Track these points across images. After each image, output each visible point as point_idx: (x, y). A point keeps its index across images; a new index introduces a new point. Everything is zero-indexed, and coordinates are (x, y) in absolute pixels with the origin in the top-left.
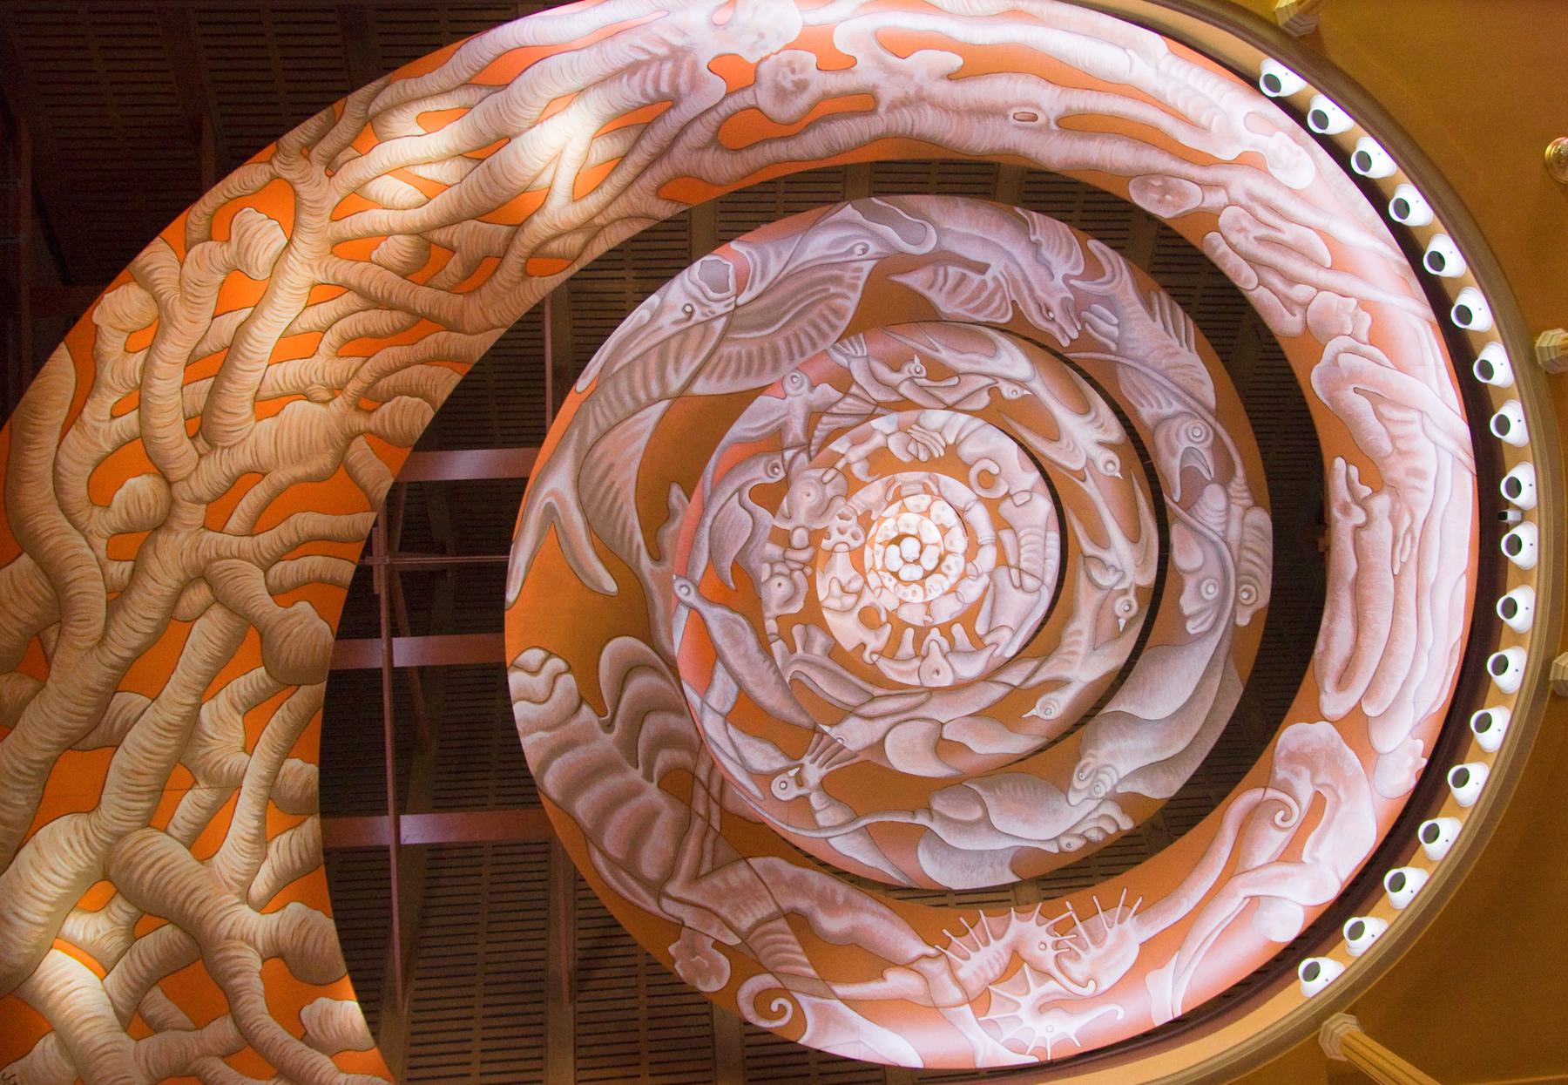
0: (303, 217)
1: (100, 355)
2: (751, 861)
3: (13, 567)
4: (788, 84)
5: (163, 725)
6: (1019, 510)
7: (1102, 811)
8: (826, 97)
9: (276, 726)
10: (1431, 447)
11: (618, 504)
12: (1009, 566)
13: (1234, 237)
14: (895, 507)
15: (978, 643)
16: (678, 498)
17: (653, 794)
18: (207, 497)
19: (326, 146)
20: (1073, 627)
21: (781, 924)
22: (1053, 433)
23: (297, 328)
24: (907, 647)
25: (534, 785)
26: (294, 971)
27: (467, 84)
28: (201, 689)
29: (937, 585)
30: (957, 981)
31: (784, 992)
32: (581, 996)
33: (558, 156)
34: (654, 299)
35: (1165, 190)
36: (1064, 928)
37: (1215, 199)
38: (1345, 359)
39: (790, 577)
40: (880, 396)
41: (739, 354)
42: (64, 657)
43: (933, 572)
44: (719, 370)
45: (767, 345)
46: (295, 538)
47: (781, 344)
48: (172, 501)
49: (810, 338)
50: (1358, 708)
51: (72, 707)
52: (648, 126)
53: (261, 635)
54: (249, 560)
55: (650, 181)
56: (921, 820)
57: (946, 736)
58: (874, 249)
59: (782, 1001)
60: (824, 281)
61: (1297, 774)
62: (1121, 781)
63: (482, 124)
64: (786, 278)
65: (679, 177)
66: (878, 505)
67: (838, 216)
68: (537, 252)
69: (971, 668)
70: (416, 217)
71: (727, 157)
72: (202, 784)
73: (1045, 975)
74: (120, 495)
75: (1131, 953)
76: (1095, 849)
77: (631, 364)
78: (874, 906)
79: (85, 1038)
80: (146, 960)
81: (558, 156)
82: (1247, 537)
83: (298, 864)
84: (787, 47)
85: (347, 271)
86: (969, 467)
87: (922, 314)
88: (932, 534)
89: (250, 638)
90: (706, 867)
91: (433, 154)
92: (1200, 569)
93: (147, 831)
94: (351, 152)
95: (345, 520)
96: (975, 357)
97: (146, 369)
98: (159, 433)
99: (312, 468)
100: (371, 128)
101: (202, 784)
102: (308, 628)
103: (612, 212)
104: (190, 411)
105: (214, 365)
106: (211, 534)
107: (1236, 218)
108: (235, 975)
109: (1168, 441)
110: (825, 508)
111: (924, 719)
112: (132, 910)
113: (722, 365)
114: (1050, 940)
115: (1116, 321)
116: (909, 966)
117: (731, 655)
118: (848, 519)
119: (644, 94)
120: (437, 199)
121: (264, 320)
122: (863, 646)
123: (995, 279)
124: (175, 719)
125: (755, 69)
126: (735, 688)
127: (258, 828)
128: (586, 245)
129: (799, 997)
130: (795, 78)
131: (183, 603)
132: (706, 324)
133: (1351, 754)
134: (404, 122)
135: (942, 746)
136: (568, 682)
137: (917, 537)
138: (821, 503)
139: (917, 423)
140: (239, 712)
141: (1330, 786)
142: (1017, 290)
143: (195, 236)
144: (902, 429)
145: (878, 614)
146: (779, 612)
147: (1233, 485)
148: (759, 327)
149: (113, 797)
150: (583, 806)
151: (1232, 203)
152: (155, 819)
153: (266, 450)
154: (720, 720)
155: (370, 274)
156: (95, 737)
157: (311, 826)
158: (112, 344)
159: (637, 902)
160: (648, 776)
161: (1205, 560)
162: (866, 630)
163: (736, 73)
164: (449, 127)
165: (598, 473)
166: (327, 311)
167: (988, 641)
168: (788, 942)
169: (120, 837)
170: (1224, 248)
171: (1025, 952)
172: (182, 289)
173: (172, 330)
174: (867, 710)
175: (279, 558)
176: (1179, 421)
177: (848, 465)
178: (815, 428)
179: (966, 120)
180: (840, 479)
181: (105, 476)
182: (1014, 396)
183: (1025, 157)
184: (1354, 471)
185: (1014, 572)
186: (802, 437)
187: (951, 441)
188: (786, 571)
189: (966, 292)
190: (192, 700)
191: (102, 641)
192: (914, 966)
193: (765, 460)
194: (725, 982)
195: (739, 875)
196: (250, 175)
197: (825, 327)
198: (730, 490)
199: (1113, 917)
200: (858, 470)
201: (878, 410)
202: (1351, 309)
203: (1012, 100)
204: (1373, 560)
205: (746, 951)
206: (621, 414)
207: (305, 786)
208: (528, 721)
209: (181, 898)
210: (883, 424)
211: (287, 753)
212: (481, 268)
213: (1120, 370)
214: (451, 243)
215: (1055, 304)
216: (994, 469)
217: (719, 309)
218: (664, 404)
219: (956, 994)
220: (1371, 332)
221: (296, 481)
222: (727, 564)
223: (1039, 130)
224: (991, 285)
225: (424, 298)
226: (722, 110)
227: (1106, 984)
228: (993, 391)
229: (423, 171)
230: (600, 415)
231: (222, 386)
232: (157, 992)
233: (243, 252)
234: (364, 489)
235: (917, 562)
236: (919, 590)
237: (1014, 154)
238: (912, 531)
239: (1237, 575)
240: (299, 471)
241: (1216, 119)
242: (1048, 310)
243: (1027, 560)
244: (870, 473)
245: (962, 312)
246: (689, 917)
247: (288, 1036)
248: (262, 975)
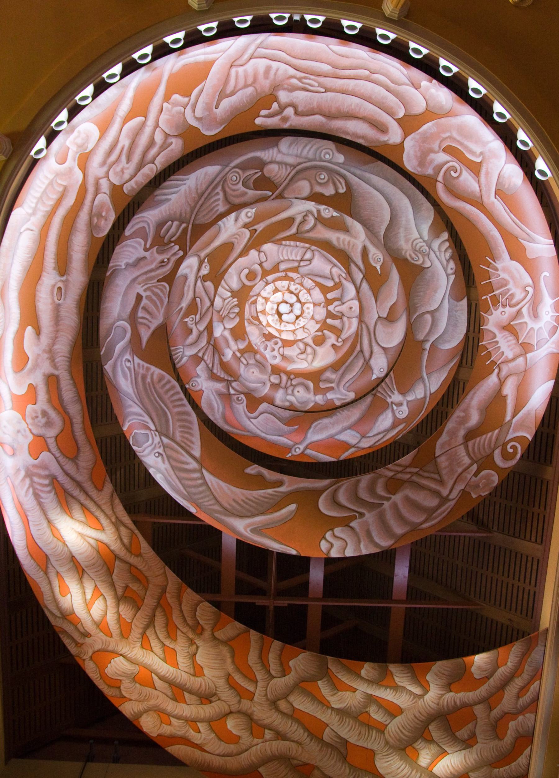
0: (110, 648)
1: (171, 735)
2: (436, 455)
3: (264, 774)
4: (44, 421)
5: (339, 723)
6: (269, 258)
7: (436, 249)
8: (50, 401)
9: (345, 678)
10: (253, 61)
11: (254, 499)
12: (299, 266)
13: (127, 176)
14: (262, 318)
15: (338, 285)
16: (252, 470)
17: (397, 498)
18: (239, 698)
19: (76, 636)
20: (335, 242)
21: (470, 444)
22: (228, 246)
23: (162, 656)
24: (336, 323)
25: (387, 551)
26: (458, 679)
27: (46, 573)
28: (325, 707)
29: (304, 296)
30: (514, 359)
31: (505, 445)
32: (490, 525)
33: (81, 535)
34: (151, 471)
35: (99, 216)
36: (496, 301)
37: (105, 185)
38: (198, 113)
39: (295, 386)
41: (181, 432)
42: (305, 758)
43: (298, 297)
45: (177, 417)
46: (260, 664)
47: (176, 410)
48: (239, 712)
49: (173, 395)
50: (399, 121)
51: (327, 757)
52: (65, 491)
53: (303, 681)
54: (269, 683)
55: (93, 493)
56: (427, 346)
57: (385, 315)
58: (128, 356)
59: (509, 447)
61: (432, 161)
63: (67, 567)
65: (91, 479)
66: (260, 330)
67: (111, 374)
68: (128, 549)
70: (111, 601)
71: (81, 454)
72: (368, 709)
73: (519, 313)
74: (234, 732)
75: (516, 266)
76: (456, 254)
77: (183, 485)
78: (468, 397)
79: (473, 762)
80: (443, 737)
81: (81, 535)
82: (295, 152)
83: (409, 675)
84: (24, 419)
85: (136, 633)
86: (244, 285)
87: (163, 334)
88: (278, 296)
89: (304, 685)
90: (436, 476)
91: (80, 591)
92: (310, 182)
93: (386, 732)
94: (79, 626)
95: (252, 642)
97: (178, 718)
98: (207, 714)
99: (228, 655)
100: (68, 616)
101: (368, 709)
102: (302, 662)
103: (109, 512)
104: (199, 702)
105: (177, 690)
106: (255, 698)
107: (116, 173)
108: (455, 703)
110: (261, 365)
112: (420, 741)
113: (186, 441)
114: (501, 309)
115: (170, 223)
116: (502, 383)
117: (332, 431)
118: (267, 346)
119: (50, 492)
120: (102, 591)
121: (156, 668)
123: (145, 290)
124: (337, 718)
125: (36, 436)
126: (349, 431)
127: (391, 689)
129: (508, 438)
130: (40, 416)
131: (285, 711)
132: (165, 446)
133: (425, 127)
134: (65, 602)
136: (338, 531)
137: (279, 304)
138: (259, 367)
140: (337, 693)
141: (441, 141)
142: (152, 278)
143: (118, 693)
144: (222, 320)
146: (312, 393)
147: (265, 158)
148: (167, 421)
149: (369, 744)
150: (399, 530)
151: (107, 176)
152: (381, 729)
153: (217, 673)
154: (364, 440)
155: (137, 623)
156: (342, 749)
157: (393, 668)
158: (166, 730)
159: (449, 509)
160: (388, 499)
161: (305, 179)
162: (326, 343)
163: (38, 445)
164: (67, 582)
165: (239, 508)
166: (154, 643)
167: (337, 280)
168: (480, 441)
169: (387, 743)
170: (132, 183)
171: (505, 323)
172: (143, 701)
173: (161, 706)
174: (367, 354)
175: (268, 672)
176: (227, 189)
177: (239, 351)
178: (219, 377)
179: (61, 327)
180: (246, 355)
181: (225, 737)
182: (208, 267)
183: (81, 296)
184: (264, 112)
186: (224, 384)
187: (229, 294)
188: (292, 388)
189: (152, 308)
190: (330, 711)
191: (298, 743)
192: (502, 380)
193: (234, 404)
194: (496, 474)
195: (443, 462)
196: (90, 669)
197: (168, 387)
199: (494, 274)
200: (242, 346)
201: (212, 343)
202: (170, 106)
203: (50, 301)
204: (315, 104)
205: (480, 461)
206: (208, 493)
207: (373, 668)
208: (355, 551)
209: (418, 722)
211: (358, 676)
212: (135, 574)
213: (197, 222)
214: (123, 587)
215: (159, 258)
216: (246, 271)
217: (157, 439)
219: (520, 360)
220: (183, 95)
221: (233, 662)
222: (286, 428)
223: (66, 286)
224: (148, 293)
225: (149, 601)
226: (58, 455)
227: (529, 280)
228: (205, 279)
229: (89, 596)
230: (208, 502)
231: (188, 689)
232: (457, 734)
233: (127, 676)
234: (238, 635)
235: (292, 305)
237: (79, 302)
238: (275, 306)
239: (315, 160)
240: (229, 661)
241: (59, 182)
242: (163, 262)
243: (296, 257)
244: (244, 340)
245: (162, 311)
246: (460, 487)
247: (487, 684)
248: (457, 693)
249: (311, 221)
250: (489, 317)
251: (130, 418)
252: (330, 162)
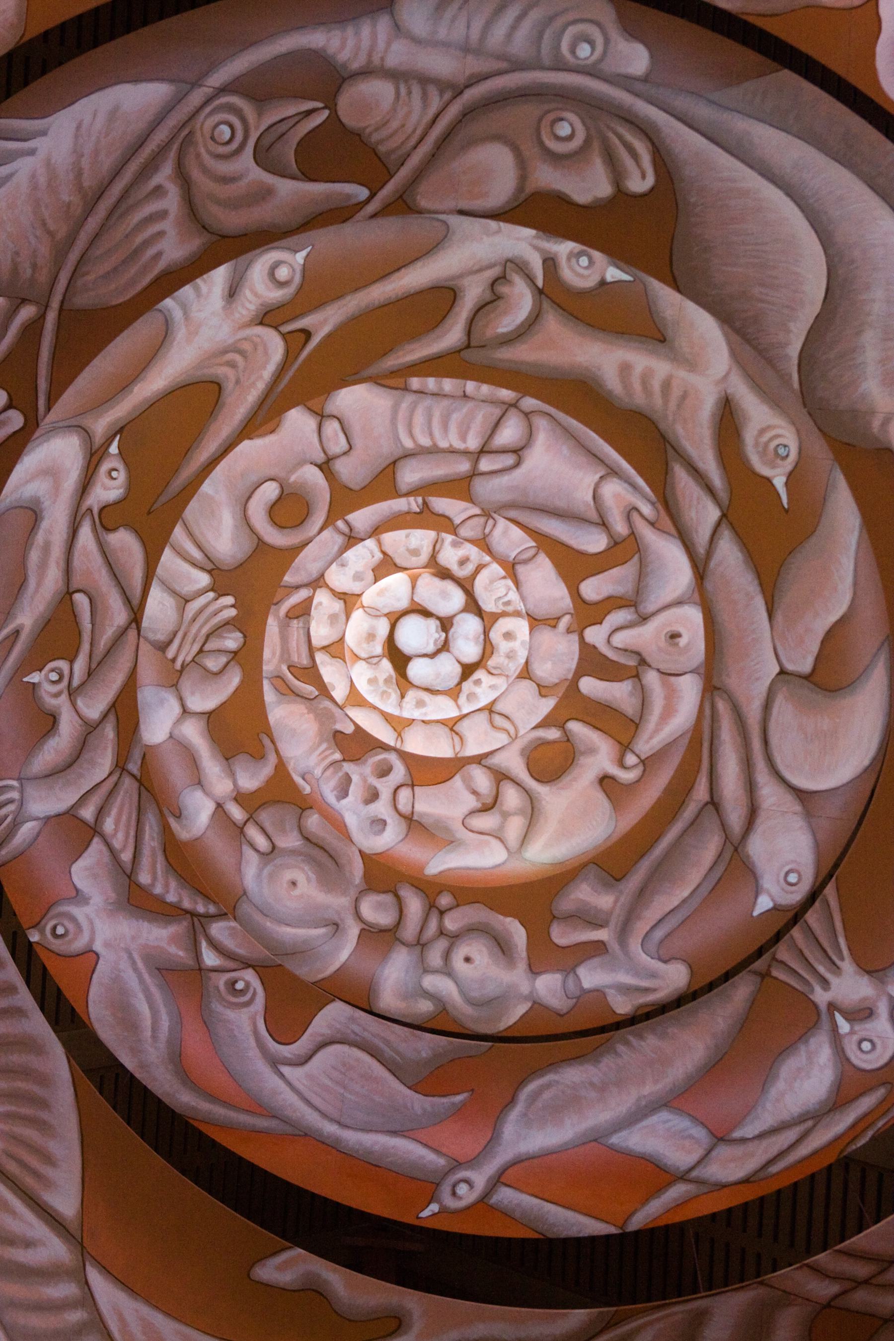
6: (358, 442)
12: (474, 473)
15: (625, 549)
16: (280, 1268)
20: (612, 382)
22: (200, 396)
24: (618, 693)
29: (493, 589)
39: (455, 938)
40: (103, 763)
43: (469, 593)
44: (34, 1162)
57: (805, 665)
66: (324, 718)
69: (674, 570)
82: (458, 33)
86: (261, 546)
88: (395, 589)
109: (234, 204)
110: (324, 856)
111: (767, 707)
117: (599, 1116)
118: (348, 779)
122: (605, 781)
126: (664, 1115)
135: (827, 677)
137: (395, 619)
139: (163, 647)
144: (173, 679)
145: (543, 743)
147: (344, 56)
154: (723, 1151)
162: (575, 772)
167: (620, 528)
174: (735, 817)
176: (196, 174)
177: (240, 798)
180: (265, 816)
182: (121, 476)
185: (485, 465)
187: (203, 579)
188: (441, 945)
198: (271, 1081)
200: (251, 779)
201: (134, 767)
210: (159, 722)
213: (82, 300)
216: (270, 491)
218: (94, 1276)
222: (418, 1103)
228: (108, 519)
235: (446, 624)
236: (504, 625)
243: (463, 438)
244: (259, 756)
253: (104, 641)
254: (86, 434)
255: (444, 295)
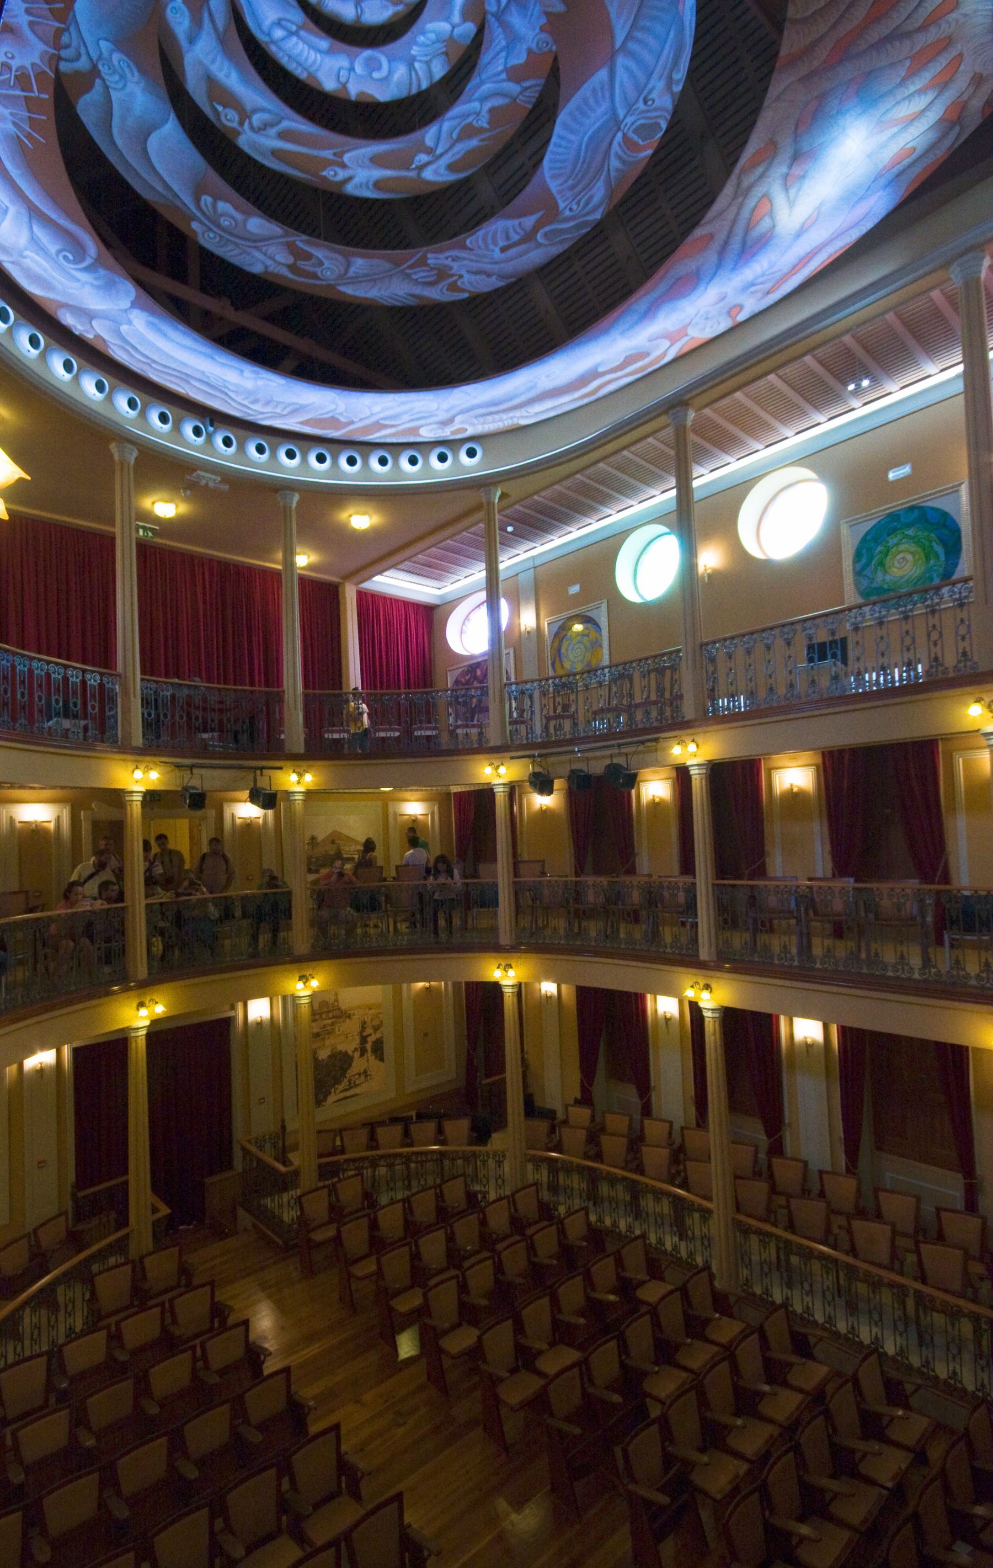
7: (84, 58)
47: (572, 137)
60: (578, 184)
62: (107, 88)
64: (603, 164)
67: (601, 210)
96: (458, 157)
103: (733, 209)
114: (15, 64)
128: (739, 185)
178: (504, 32)
182: (417, 158)
185: (294, 28)
215: (455, 265)
216: (376, 75)
224: (491, 247)
249: (257, 119)
250: (38, 61)
251: (631, 159)
252: (210, 229)
253: (457, 121)
254: (419, 174)
255: (283, 136)
